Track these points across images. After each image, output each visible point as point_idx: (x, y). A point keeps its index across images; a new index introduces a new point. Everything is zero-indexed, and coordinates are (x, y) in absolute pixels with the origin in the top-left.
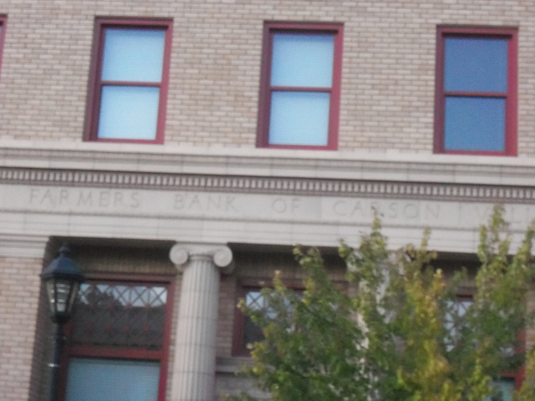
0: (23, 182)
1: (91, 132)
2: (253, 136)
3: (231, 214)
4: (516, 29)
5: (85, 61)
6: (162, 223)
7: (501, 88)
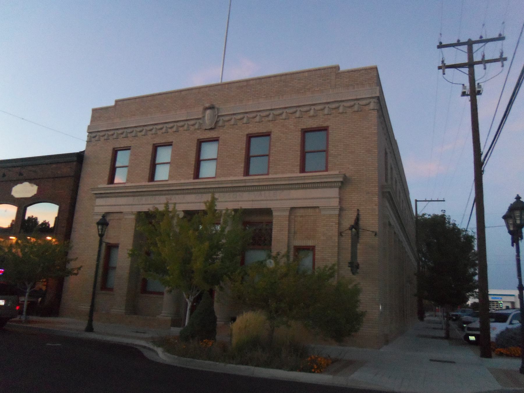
0: (131, 196)
1: (197, 175)
2: (192, 176)
3: (184, 201)
4: (271, 132)
5: (149, 157)
6: (102, 207)
7: (323, 148)
